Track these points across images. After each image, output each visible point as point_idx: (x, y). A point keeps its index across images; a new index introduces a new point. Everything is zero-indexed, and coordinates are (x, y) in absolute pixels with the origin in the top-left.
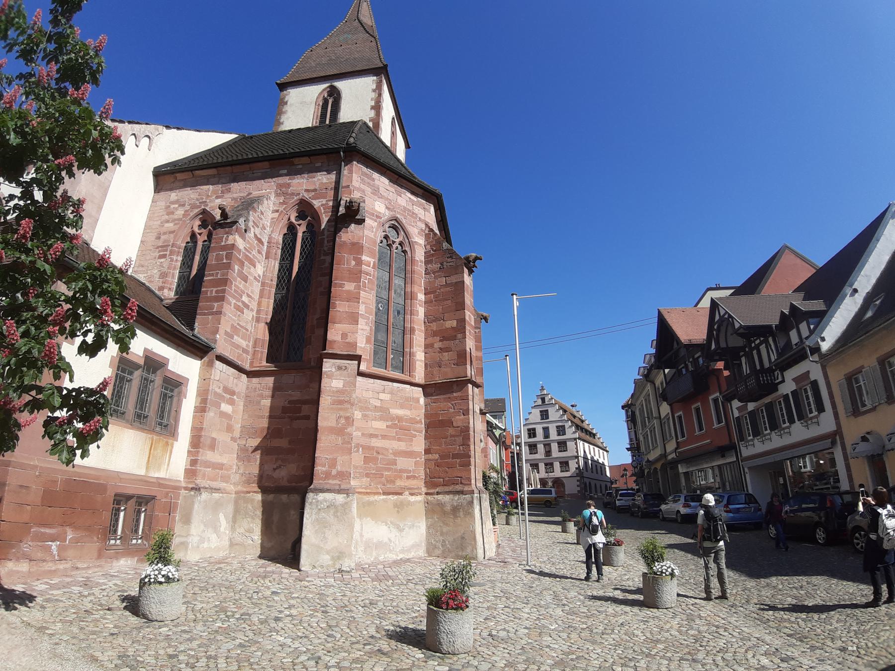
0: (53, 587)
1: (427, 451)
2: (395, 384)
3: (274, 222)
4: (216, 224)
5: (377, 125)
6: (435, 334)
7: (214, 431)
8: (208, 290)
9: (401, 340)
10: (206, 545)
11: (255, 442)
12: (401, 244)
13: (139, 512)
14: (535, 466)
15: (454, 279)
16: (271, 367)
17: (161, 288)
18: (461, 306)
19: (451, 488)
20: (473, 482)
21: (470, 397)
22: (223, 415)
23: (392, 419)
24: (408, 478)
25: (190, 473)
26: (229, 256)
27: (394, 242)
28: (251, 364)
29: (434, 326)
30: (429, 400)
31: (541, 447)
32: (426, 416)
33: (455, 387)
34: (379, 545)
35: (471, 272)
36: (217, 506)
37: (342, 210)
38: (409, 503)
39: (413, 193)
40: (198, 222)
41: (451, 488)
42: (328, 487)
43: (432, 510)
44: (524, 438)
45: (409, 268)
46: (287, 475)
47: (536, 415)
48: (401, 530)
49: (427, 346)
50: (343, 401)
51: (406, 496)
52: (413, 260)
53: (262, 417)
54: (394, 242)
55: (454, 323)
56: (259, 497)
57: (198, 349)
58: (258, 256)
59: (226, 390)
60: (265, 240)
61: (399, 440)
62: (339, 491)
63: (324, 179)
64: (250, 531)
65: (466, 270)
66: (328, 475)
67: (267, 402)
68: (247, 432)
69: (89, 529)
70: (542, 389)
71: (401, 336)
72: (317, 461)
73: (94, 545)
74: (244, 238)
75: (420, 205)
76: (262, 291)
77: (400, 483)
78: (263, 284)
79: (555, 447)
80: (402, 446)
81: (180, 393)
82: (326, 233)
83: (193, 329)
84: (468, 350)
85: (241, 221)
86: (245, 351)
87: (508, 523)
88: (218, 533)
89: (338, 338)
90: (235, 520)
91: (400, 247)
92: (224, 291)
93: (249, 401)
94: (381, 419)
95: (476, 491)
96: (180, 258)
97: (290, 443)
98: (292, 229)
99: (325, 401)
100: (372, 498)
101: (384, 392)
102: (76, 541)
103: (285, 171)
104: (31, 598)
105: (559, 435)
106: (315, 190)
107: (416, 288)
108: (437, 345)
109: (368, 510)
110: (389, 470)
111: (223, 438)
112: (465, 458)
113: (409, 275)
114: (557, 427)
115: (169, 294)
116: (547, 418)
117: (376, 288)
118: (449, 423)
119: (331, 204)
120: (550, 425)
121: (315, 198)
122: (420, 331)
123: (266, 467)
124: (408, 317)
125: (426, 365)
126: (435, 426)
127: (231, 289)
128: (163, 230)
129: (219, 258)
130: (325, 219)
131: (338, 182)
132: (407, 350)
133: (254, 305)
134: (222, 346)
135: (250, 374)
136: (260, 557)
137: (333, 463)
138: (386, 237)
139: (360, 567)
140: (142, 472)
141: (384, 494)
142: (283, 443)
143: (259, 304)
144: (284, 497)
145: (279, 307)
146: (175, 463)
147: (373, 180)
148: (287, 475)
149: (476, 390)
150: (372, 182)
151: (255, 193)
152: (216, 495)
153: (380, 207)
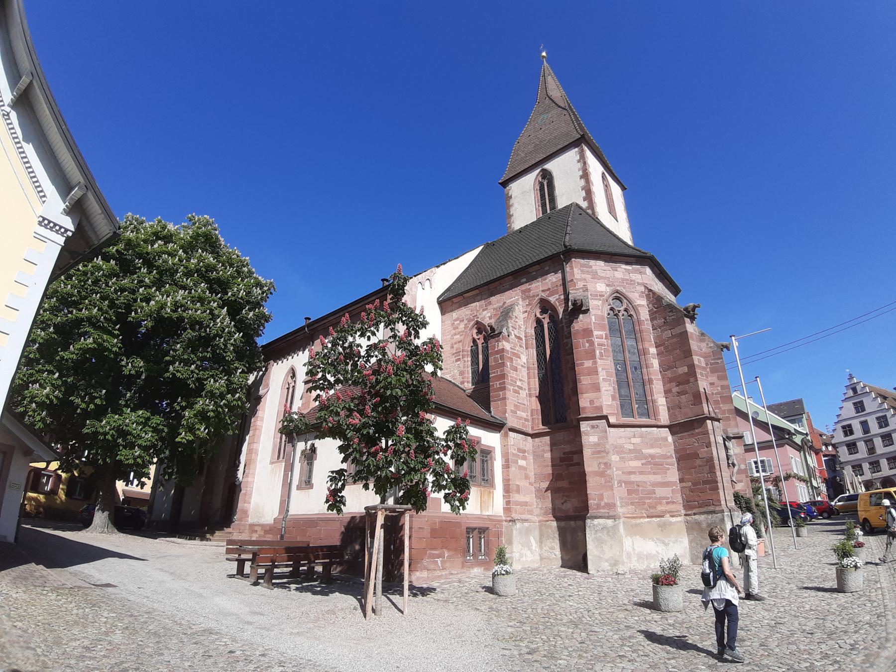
0: (442, 584)
1: (681, 480)
2: (643, 429)
3: (526, 321)
4: (489, 334)
5: (591, 205)
6: (671, 380)
7: (518, 481)
8: (494, 384)
9: (642, 391)
10: (524, 559)
11: (545, 485)
12: (626, 310)
13: (480, 538)
14: (857, 468)
15: (677, 330)
16: (546, 429)
17: (462, 383)
18: (688, 353)
19: (705, 509)
20: (723, 502)
21: (711, 432)
22: (521, 468)
23: (646, 458)
24: (668, 503)
25: (507, 510)
26: (502, 358)
27: (619, 311)
28: (532, 428)
29: (669, 374)
30: (676, 437)
31: (861, 445)
32: (676, 451)
33: (696, 424)
34: (649, 556)
35: (692, 319)
36: (528, 531)
37: (571, 307)
38: (671, 523)
39: (627, 263)
40: (475, 331)
41: (705, 509)
42: (599, 514)
43: (691, 528)
44: (840, 437)
45: (637, 328)
46: (571, 507)
47: (849, 409)
48: (666, 545)
49: (666, 392)
50: (601, 451)
51: (667, 518)
52: (639, 322)
53: (548, 466)
54: (619, 311)
55: (685, 369)
56: (555, 524)
57: (496, 426)
58: (521, 350)
59: (520, 450)
60: (523, 336)
61: (654, 474)
62: (608, 518)
63: (553, 279)
64: (553, 548)
65: (687, 320)
66: (599, 506)
67: (548, 455)
68: (539, 477)
69: (455, 549)
70: (851, 377)
71: (641, 387)
72: (589, 496)
73: (459, 560)
74: (508, 342)
75: (635, 271)
76: (528, 374)
77: (660, 508)
78: (528, 369)
79: (878, 442)
80: (658, 478)
81: (491, 458)
82: (564, 321)
83: (490, 412)
84: (702, 390)
85: (504, 330)
86: (526, 420)
87: (798, 536)
88: (532, 549)
89: (587, 405)
90: (541, 541)
91: (625, 313)
92: (504, 383)
93: (536, 456)
94: (636, 458)
95: (726, 510)
96: (470, 359)
97: (570, 483)
98: (539, 322)
99: (587, 453)
100: (638, 521)
101: (634, 436)
102: (449, 557)
103: (525, 280)
104: (435, 589)
105: (881, 427)
106: (549, 289)
107: (646, 345)
108: (675, 390)
109: (634, 531)
110: (650, 498)
111: (523, 483)
112: (713, 484)
113: (638, 335)
114: (877, 418)
115: (469, 386)
116: (863, 410)
117: (611, 354)
118: (696, 456)
119: (562, 297)
120: (869, 418)
121: (550, 295)
122: (658, 380)
123: (556, 502)
124: (644, 370)
125: (668, 408)
126: (685, 458)
127: (508, 381)
128: (454, 341)
129: (496, 360)
130: (561, 310)
131: (564, 279)
132: (649, 398)
133: (525, 386)
134: (511, 422)
135: (533, 436)
136: (562, 567)
137: (601, 497)
138: (612, 309)
139: (633, 572)
140: (479, 513)
141: (648, 517)
142: (564, 484)
143: (529, 384)
144: (572, 523)
145: (543, 383)
146: (496, 505)
147: (591, 267)
148: (571, 507)
149: (716, 423)
150: (590, 270)
151: (509, 302)
152: (526, 524)
153: (601, 287)
